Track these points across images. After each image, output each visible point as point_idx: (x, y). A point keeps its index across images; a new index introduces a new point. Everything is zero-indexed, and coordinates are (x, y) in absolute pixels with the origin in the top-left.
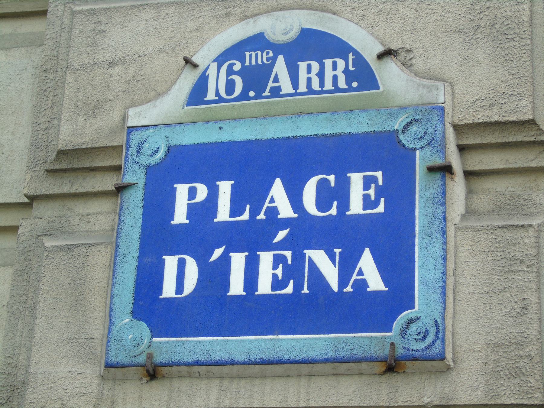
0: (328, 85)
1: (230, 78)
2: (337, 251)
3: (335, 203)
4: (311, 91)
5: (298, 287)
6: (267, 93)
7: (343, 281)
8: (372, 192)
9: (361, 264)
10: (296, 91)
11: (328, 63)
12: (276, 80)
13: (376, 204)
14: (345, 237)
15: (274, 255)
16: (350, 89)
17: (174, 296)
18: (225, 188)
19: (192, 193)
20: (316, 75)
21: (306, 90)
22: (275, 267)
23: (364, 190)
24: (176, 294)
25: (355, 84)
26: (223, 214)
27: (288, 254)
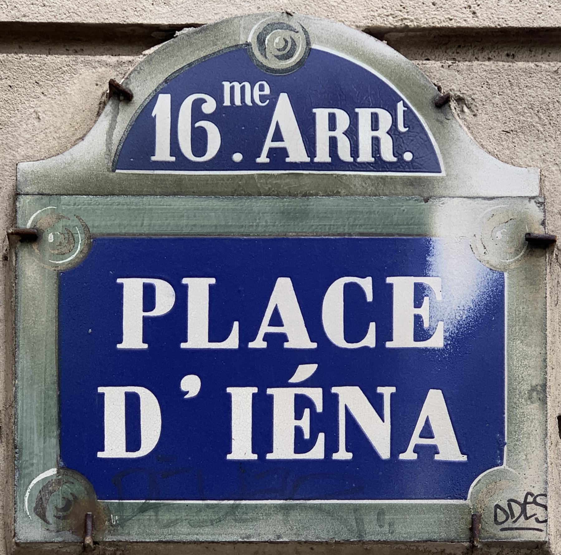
0: (365, 156)
1: (197, 125)
2: (387, 392)
4: (336, 163)
5: (331, 446)
6: (263, 159)
8: (305, 423)
10: (312, 160)
11: (364, 115)
12: (278, 137)
16: (399, 165)
20: (345, 133)
21: (329, 160)
22: (298, 416)
26: (197, 337)
27: (316, 395)
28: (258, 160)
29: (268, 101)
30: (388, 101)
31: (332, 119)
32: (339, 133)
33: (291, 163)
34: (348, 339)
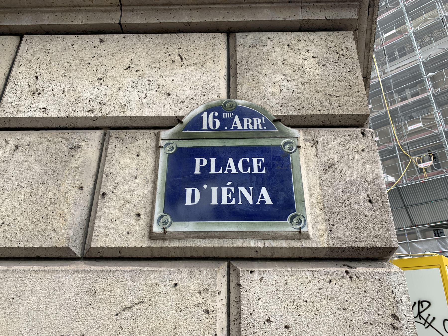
3: (222, 168)
5: (237, 201)
6: (232, 128)
7: (255, 199)
8: (230, 196)
11: (255, 120)
13: (262, 170)
14: (255, 182)
18: (213, 160)
19: (201, 162)
22: (228, 194)
24: (192, 203)
25: (265, 128)
26: (213, 171)
27: (233, 189)
30: (261, 117)
31: (248, 120)
32: (249, 123)
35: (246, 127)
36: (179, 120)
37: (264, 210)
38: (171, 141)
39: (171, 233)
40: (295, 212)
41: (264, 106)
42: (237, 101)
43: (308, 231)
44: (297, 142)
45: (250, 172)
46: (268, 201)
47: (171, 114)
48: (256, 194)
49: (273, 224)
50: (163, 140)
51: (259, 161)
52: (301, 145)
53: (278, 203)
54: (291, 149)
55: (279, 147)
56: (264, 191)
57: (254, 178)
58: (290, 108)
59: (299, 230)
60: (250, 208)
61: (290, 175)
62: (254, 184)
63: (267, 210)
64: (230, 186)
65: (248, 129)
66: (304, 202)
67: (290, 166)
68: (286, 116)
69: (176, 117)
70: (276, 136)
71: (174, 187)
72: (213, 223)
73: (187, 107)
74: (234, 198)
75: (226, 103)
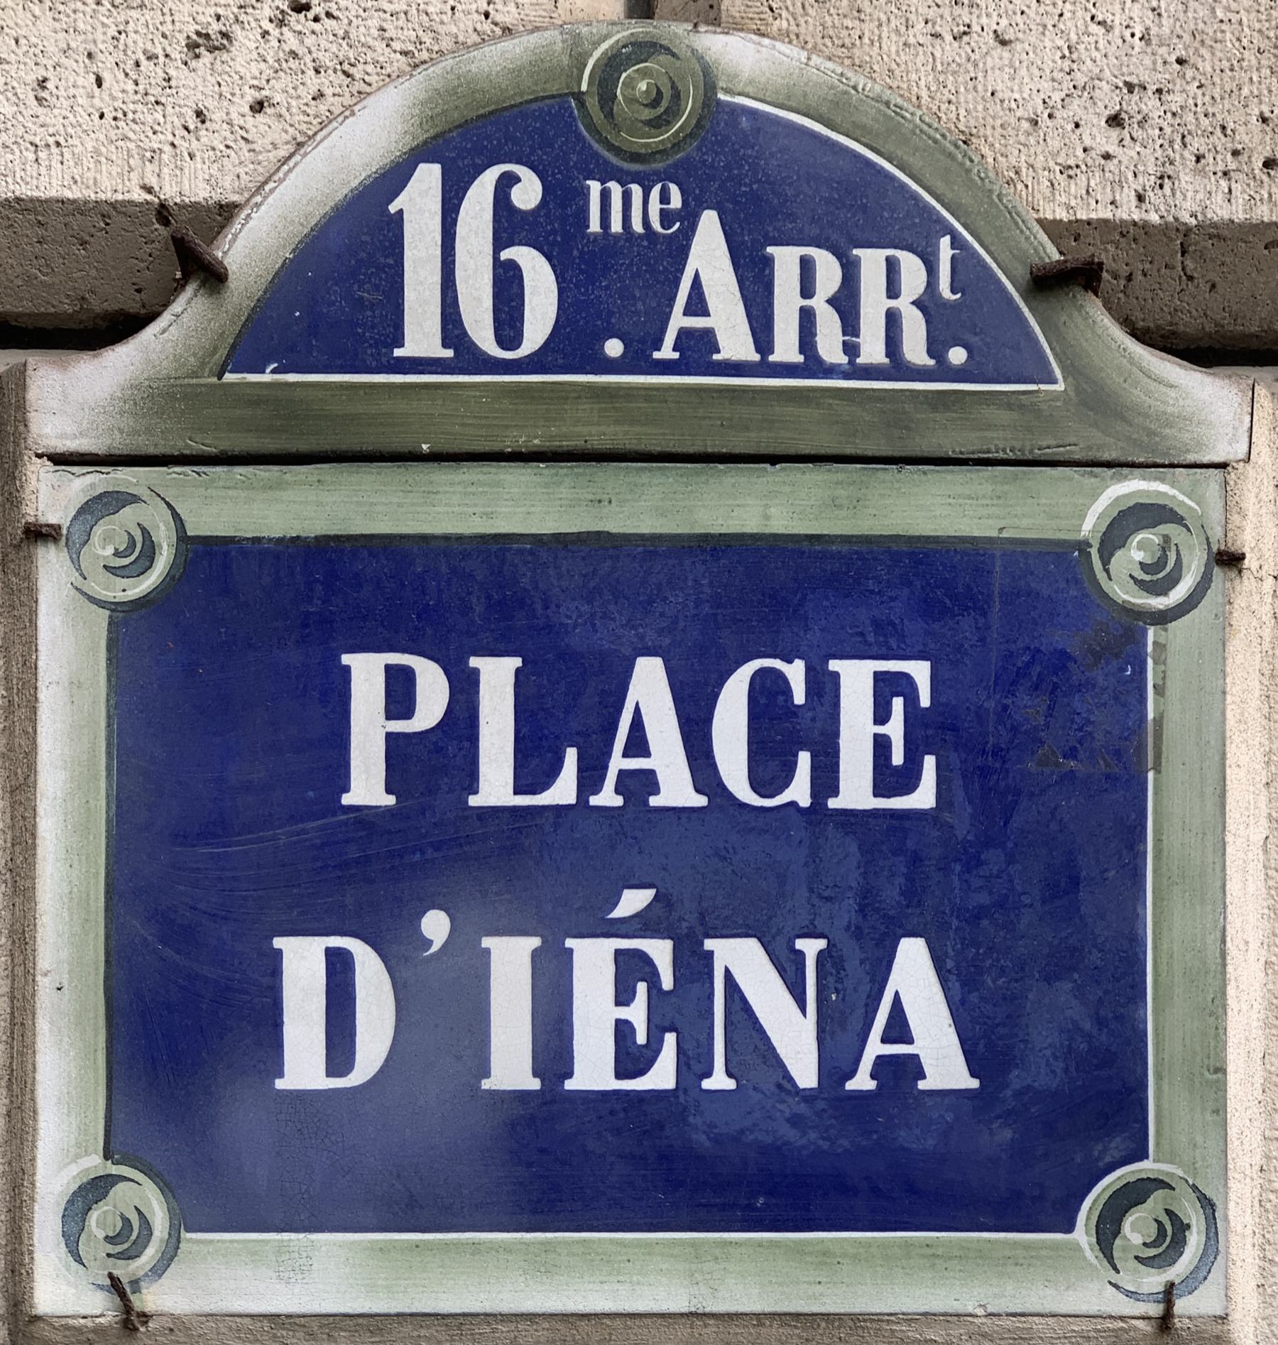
1: (505, 255)
2: (811, 947)
3: (571, 755)
5: (693, 1063)
6: (667, 352)
8: (637, 1013)
9: (809, 1025)
11: (872, 261)
12: (697, 305)
13: (905, 780)
15: (618, 953)
16: (944, 371)
17: (610, 1083)
18: (497, 677)
20: (830, 301)
22: (623, 997)
23: (390, 716)
24: (331, 1072)
25: (957, 356)
26: (495, 785)
27: (660, 951)
28: (657, 355)
29: (678, 224)
30: (918, 233)
33: (719, 363)
34: (757, 785)
35: (786, 349)
36: (184, 246)
37: (904, 1137)
38: (125, 477)
39: (177, 1325)
40: (1142, 1154)
41: (964, 111)
42: (722, 48)
43: (1224, 1318)
44: (1215, 514)
45: (805, 801)
46: (944, 1064)
47: (114, 181)
48: (847, 1002)
49: (964, 1255)
50: (60, 459)
51: (887, 687)
52: (1246, 541)
53: (1016, 1078)
54: (1158, 576)
55: (1065, 562)
56: (913, 972)
57: (845, 861)
58: (1197, 144)
59: (1155, 1310)
60: (795, 1121)
61: (1131, 832)
62: (846, 910)
63: (930, 1142)
64: (643, 924)
65: (813, 365)
66: (1221, 1070)
67: (1141, 747)
68: (1145, 226)
69: (163, 212)
70: (1046, 445)
71: (176, 931)
72: (507, 1248)
73: (258, 107)
74: (670, 1039)
75: (613, 64)
